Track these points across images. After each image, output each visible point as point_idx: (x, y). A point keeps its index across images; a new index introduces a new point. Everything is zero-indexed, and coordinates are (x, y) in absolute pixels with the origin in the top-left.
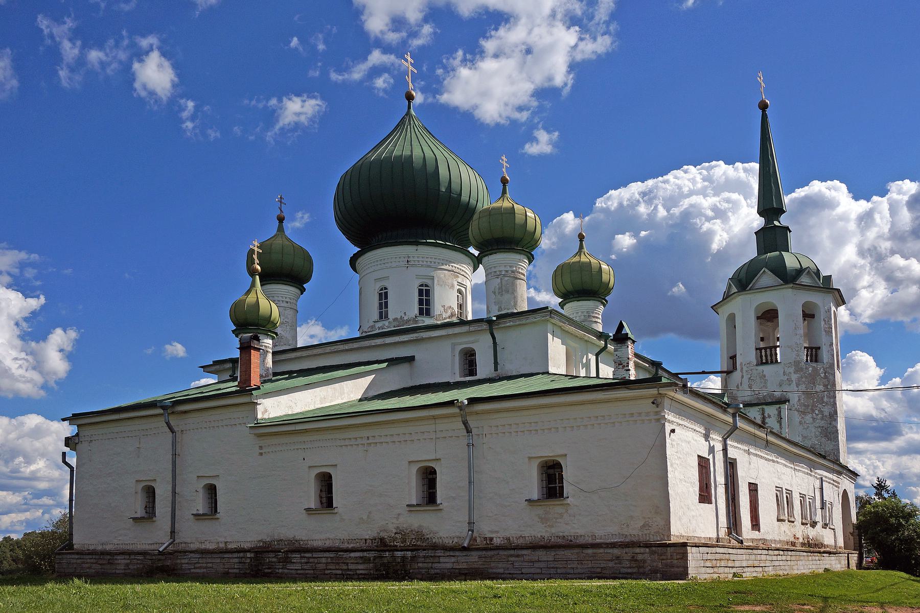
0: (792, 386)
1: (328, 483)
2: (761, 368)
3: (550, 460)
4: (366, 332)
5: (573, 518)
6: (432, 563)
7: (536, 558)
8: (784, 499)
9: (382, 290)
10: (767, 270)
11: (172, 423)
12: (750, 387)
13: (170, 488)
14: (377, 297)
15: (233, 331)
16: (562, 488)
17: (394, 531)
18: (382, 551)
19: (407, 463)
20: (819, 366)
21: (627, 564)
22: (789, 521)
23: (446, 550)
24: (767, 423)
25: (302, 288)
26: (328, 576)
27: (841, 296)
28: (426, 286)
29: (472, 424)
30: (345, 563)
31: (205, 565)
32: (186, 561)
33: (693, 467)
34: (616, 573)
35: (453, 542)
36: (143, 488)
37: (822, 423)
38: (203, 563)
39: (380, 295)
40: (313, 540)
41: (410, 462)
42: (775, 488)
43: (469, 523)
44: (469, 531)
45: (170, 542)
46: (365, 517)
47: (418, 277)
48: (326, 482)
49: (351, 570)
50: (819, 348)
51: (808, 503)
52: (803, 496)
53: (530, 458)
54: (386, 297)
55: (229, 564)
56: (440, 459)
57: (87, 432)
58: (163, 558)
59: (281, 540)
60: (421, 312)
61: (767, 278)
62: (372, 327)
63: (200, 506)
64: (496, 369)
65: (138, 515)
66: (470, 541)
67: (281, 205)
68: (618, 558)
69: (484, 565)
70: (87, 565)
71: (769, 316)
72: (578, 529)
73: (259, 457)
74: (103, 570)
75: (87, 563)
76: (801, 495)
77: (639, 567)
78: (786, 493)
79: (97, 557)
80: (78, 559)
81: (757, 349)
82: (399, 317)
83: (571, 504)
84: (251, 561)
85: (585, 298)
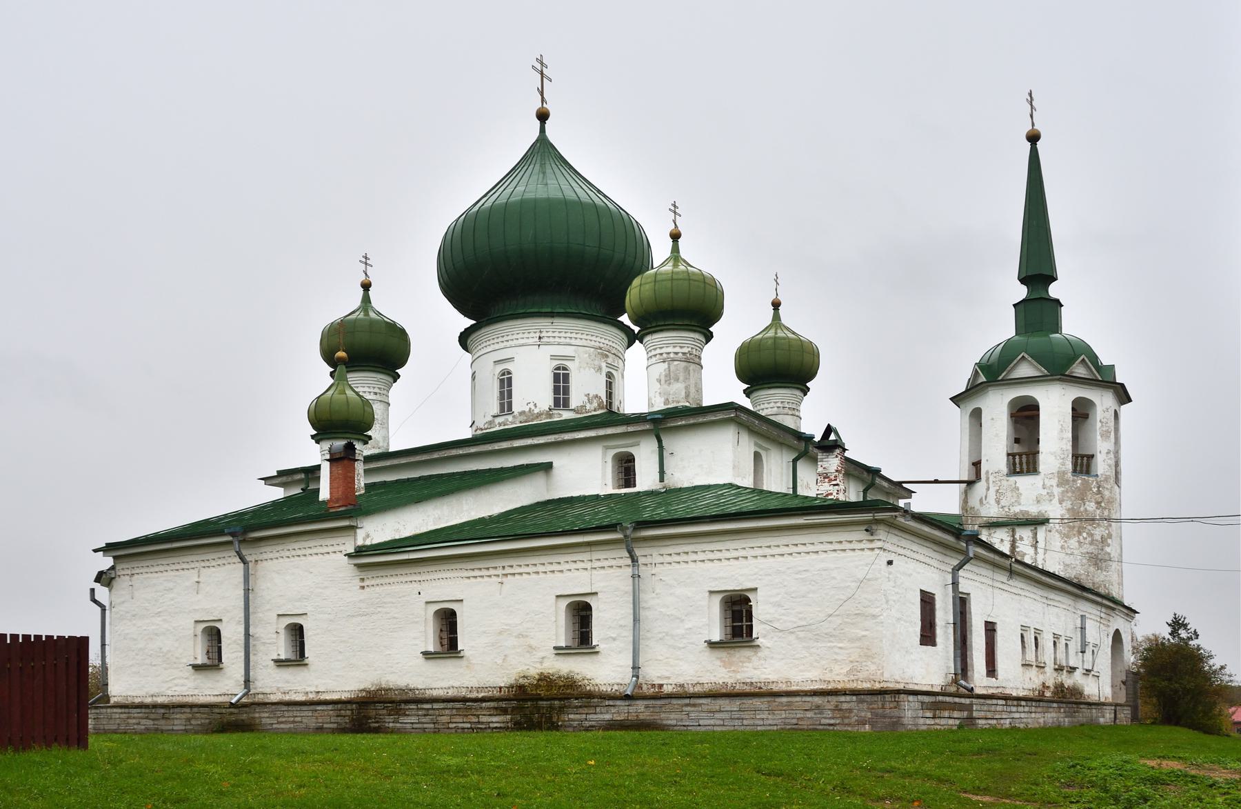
0: (1053, 502)
1: (450, 622)
2: (1013, 479)
4: (482, 429)
5: (763, 662)
6: (587, 714)
7: (718, 708)
8: (1030, 639)
9: (503, 374)
10: (1026, 356)
11: (244, 552)
12: (998, 502)
13: (241, 629)
14: (496, 384)
15: (313, 437)
16: (750, 628)
17: (537, 677)
18: (523, 700)
19: (555, 597)
23: (605, 698)
24: (1018, 547)
25: (394, 374)
26: (453, 731)
28: (565, 369)
29: (638, 552)
30: (475, 715)
32: (267, 715)
33: (913, 604)
34: (815, 725)
35: (612, 689)
37: (1091, 549)
39: (502, 381)
41: (557, 596)
42: (1020, 628)
43: (633, 668)
44: (633, 676)
46: (500, 662)
47: (553, 357)
48: (448, 621)
49: (483, 723)
50: (1092, 456)
52: (1056, 637)
53: (711, 592)
54: (510, 384)
58: (235, 711)
59: (390, 689)
60: (557, 402)
62: (490, 423)
63: (282, 649)
64: (662, 480)
65: (199, 662)
66: (634, 689)
68: (818, 707)
69: (652, 716)
70: (134, 721)
74: (156, 726)
75: (134, 718)
77: (843, 718)
79: (147, 711)
80: (121, 713)
81: (1008, 455)
82: (527, 410)
83: (761, 645)
84: (353, 713)
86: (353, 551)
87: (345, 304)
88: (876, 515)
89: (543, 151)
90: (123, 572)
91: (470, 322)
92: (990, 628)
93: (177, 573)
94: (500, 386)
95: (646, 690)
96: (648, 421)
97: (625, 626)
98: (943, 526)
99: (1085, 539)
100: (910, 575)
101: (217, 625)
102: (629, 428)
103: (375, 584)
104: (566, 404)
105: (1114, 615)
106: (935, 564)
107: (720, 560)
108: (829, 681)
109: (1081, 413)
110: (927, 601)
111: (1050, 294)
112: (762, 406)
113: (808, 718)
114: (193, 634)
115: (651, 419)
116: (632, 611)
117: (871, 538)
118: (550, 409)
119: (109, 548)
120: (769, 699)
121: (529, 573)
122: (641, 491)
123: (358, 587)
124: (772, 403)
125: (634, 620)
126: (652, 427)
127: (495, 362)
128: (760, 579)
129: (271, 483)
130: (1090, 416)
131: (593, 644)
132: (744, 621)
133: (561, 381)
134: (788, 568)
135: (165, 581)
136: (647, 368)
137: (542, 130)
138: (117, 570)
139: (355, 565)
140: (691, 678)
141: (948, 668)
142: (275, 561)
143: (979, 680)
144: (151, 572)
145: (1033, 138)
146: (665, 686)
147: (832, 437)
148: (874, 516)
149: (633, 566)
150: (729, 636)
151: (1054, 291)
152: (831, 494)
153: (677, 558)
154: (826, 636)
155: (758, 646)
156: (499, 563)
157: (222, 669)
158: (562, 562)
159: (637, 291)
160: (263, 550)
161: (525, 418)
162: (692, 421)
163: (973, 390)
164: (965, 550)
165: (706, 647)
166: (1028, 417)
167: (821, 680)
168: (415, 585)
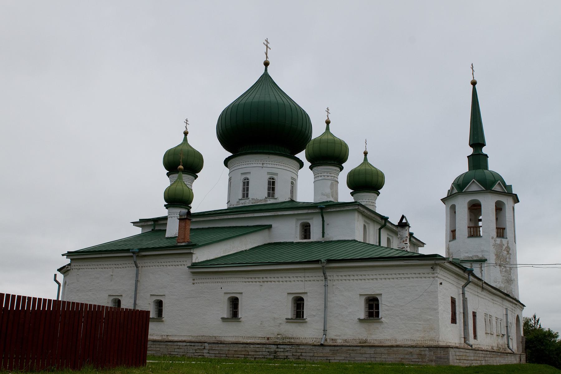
9: (245, 180)
11: (138, 262)
14: (241, 184)
15: (165, 206)
20: (504, 241)
21: (415, 356)
22: (491, 334)
28: (273, 179)
29: (328, 274)
31: (155, 349)
33: (449, 303)
35: (313, 341)
38: (153, 348)
39: (244, 183)
40: (225, 337)
41: (288, 293)
47: (269, 173)
48: (234, 303)
50: (504, 229)
51: (489, 319)
53: (361, 295)
54: (248, 185)
55: (171, 349)
57: (75, 265)
60: (269, 195)
61: (474, 187)
64: (323, 236)
67: (186, 125)
72: (387, 336)
73: (192, 285)
76: (496, 319)
78: (490, 317)
85: (369, 191)
86: (190, 265)
87: (176, 141)
88: (436, 261)
89: (266, 79)
90: (74, 267)
91: (231, 154)
92: (474, 315)
93: (101, 270)
94: (243, 185)
95: (329, 343)
97: (319, 310)
98: (460, 267)
101: (120, 298)
102: (309, 211)
103: (197, 282)
105: (516, 308)
108: (415, 340)
109: (499, 208)
110: (453, 302)
111: (483, 151)
112: (364, 200)
113: (406, 358)
115: (319, 208)
116: (324, 302)
117: (433, 272)
118: (266, 198)
119: (69, 254)
120: (388, 348)
125: (325, 307)
126: (320, 211)
127: (241, 173)
130: (503, 209)
132: (374, 309)
133: (272, 185)
134: (396, 285)
135: (95, 273)
136: (314, 182)
137: (266, 70)
138: (72, 266)
141: (461, 335)
142: (151, 267)
143: (472, 341)
146: (338, 340)
147: (404, 221)
148: (435, 262)
149: (325, 281)
151: (485, 150)
152: (404, 248)
154: (413, 318)
155: (382, 322)
156: (261, 275)
161: (254, 201)
162: (338, 209)
163: (451, 196)
164: (468, 278)
167: (411, 340)
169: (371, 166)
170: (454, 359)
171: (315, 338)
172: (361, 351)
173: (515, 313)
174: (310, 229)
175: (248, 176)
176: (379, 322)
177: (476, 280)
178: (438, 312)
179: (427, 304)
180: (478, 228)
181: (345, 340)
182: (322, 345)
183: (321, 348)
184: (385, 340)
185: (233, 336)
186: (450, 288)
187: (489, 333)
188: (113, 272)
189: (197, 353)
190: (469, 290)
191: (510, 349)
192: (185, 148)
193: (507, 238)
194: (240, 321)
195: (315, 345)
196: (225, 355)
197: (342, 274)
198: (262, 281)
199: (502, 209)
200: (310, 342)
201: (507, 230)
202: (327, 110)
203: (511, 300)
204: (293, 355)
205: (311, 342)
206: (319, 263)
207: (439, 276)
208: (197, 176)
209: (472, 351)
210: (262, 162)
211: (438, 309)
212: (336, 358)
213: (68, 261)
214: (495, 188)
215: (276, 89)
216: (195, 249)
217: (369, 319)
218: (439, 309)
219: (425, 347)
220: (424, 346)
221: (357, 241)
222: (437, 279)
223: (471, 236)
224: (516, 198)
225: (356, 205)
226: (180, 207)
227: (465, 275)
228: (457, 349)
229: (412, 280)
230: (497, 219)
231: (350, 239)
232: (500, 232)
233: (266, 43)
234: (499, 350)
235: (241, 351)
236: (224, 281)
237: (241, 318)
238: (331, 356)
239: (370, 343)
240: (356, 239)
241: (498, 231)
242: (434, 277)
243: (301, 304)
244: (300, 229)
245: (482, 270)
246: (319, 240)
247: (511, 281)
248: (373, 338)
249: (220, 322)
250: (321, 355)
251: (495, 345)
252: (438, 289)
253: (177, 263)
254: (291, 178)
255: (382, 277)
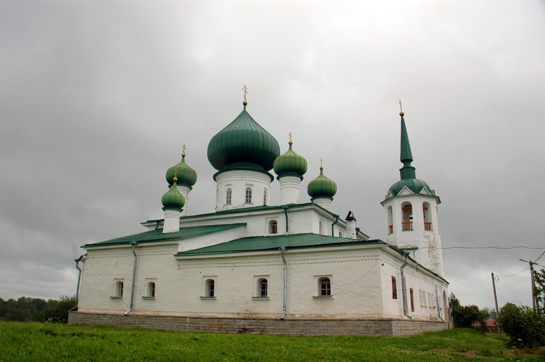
3: (323, 278)
9: (228, 190)
11: (136, 252)
13: (131, 283)
14: (226, 193)
15: (163, 208)
19: (253, 276)
22: (425, 307)
27: (439, 200)
29: (286, 259)
33: (390, 282)
36: (117, 282)
39: (228, 192)
41: (254, 276)
43: (284, 307)
44: (284, 310)
45: (130, 310)
47: (246, 185)
48: (211, 284)
50: (430, 223)
54: (230, 194)
56: (269, 275)
60: (247, 201)
61: (406, 191)
63: (146, 293)
64: (287, 231)
65: (114, 296)
71: (407, 209)
73: (178, 270)
81: (402, 223)
83: (334, 298)
91: (217, 171)
92: (411, 291)
93: (110, 258)
96: (283, 209)
99: (431, 255)
100: (389, 270)
101: (122, 281)
104: (250, 202)
106: (395, 265)
107: (318, 263)
108: (361, 314)
109: (426, 208)
110: (394, 280)
114: (113, 284)
121: (243, 266)
122: (279, 235)
123: (177, 269)
124: (323, 203)
126: (284, 211)
128: (333, 271)
129: (144, 225)
130: (428, 209)
131: (268, 296)
133: (249, 194)
137: (245, 108)
139: (177, 259)
140: (306, 312)
143: (410, 313)
144: (100, 257)
145: (402, 115)
147: (351, 216)
150: (321, 294)
151: (412, 164)
153: (301, 262)
155: (333, 299)
157: (122, 299)
158: (256, 262)
159: (276, 163)
160: (142, 251)
163: (388, 200)
165: (312, 299)
166: (408, 209)
167: (358, 314)
168: (199, 269)
169: (325, 178)
170: (397, 331)
171: (277, 313)
172: (316, 325)
173: (442, 290)
174: (277, 225)
175: (230, 187)
176: (330, 299)
177: (411, 262)
178: (381, 290)
179: (372, 282)
180: (410, 223)
181: (302, 315)
182: (282, 319)
183: (282, 321)
184: (336, 314)
185: (210, 313)
186: (391, 269)
187: (423, 306)
188: (118, 260)
189: (180, 326)
190: (406, 271)
191: (440, 318)
192: (182, 166)
193: (433, 231)
194: (216, 300)
195: (276, 320)
196: (203, 328)
197: (299, 259)
198: (233, 266)
199: (428, 208)
200: (272, 317)
201: (433, 224)
202: (290, 134)
203: (439, 279)
204: (258, 328)
205: (274, 317)
206: (279, 250)
207: (381, 258)
208: (192, 188)
209: (411, 322)
210: (241, 176)
211: (381, 287)
212: (294, 330)
213: (85, 252)
214: (422, 192)
215: (252, 122)
216: (181, 241)
217: (322, 296)
218: (382, 286)
219: (371, 320)
220: (370, 320)
221: (314, 234)
222: (379, 260)
223: (412, 219)
224: (438, 199)
225: (312, 205)
226: (174, 209)
227: (403, 258)
228: (398, 321)
229: (358, 262)
230: (424, 216)
231: (309, 232)
232: (427, 226)
233: (244, 88)
234: (432, 320)
235: (216, 325)
236: (203, 266)
237: (216, 297)
238: (290, 328)
239: (323, 317)
240: (314, 232)
241: (426, 225)
242: (377, 259)
243: (265, 285)
244: (269, 226)
245: (415, 256)
246: (284, 234)
247: (438, 264)
248: (326, 313)
249: (199, 300)
250: (282, 328)
251: (428, 316)
252: (380, 269)
253: (166, 253)
254: (264, 188)
255: (332, 260)
